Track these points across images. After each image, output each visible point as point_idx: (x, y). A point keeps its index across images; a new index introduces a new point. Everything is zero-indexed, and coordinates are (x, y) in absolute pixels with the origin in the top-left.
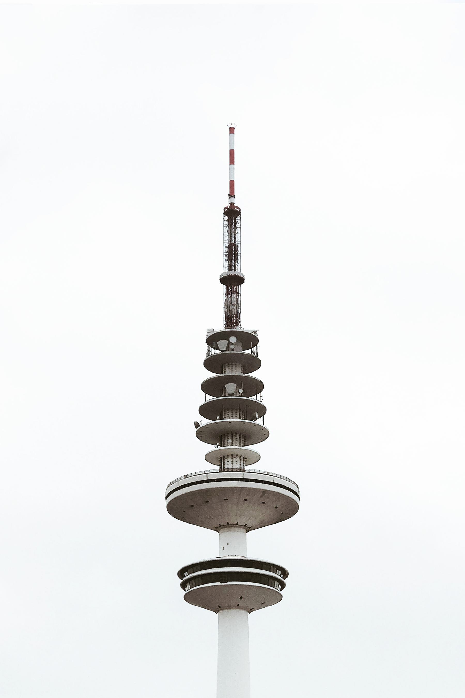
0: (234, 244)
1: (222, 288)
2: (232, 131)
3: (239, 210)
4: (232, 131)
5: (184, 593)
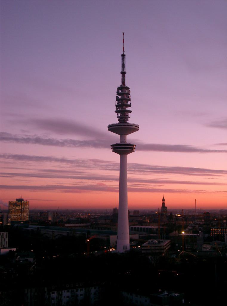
1: (121, 75)
2: (123, 34)
4: (123, 34)
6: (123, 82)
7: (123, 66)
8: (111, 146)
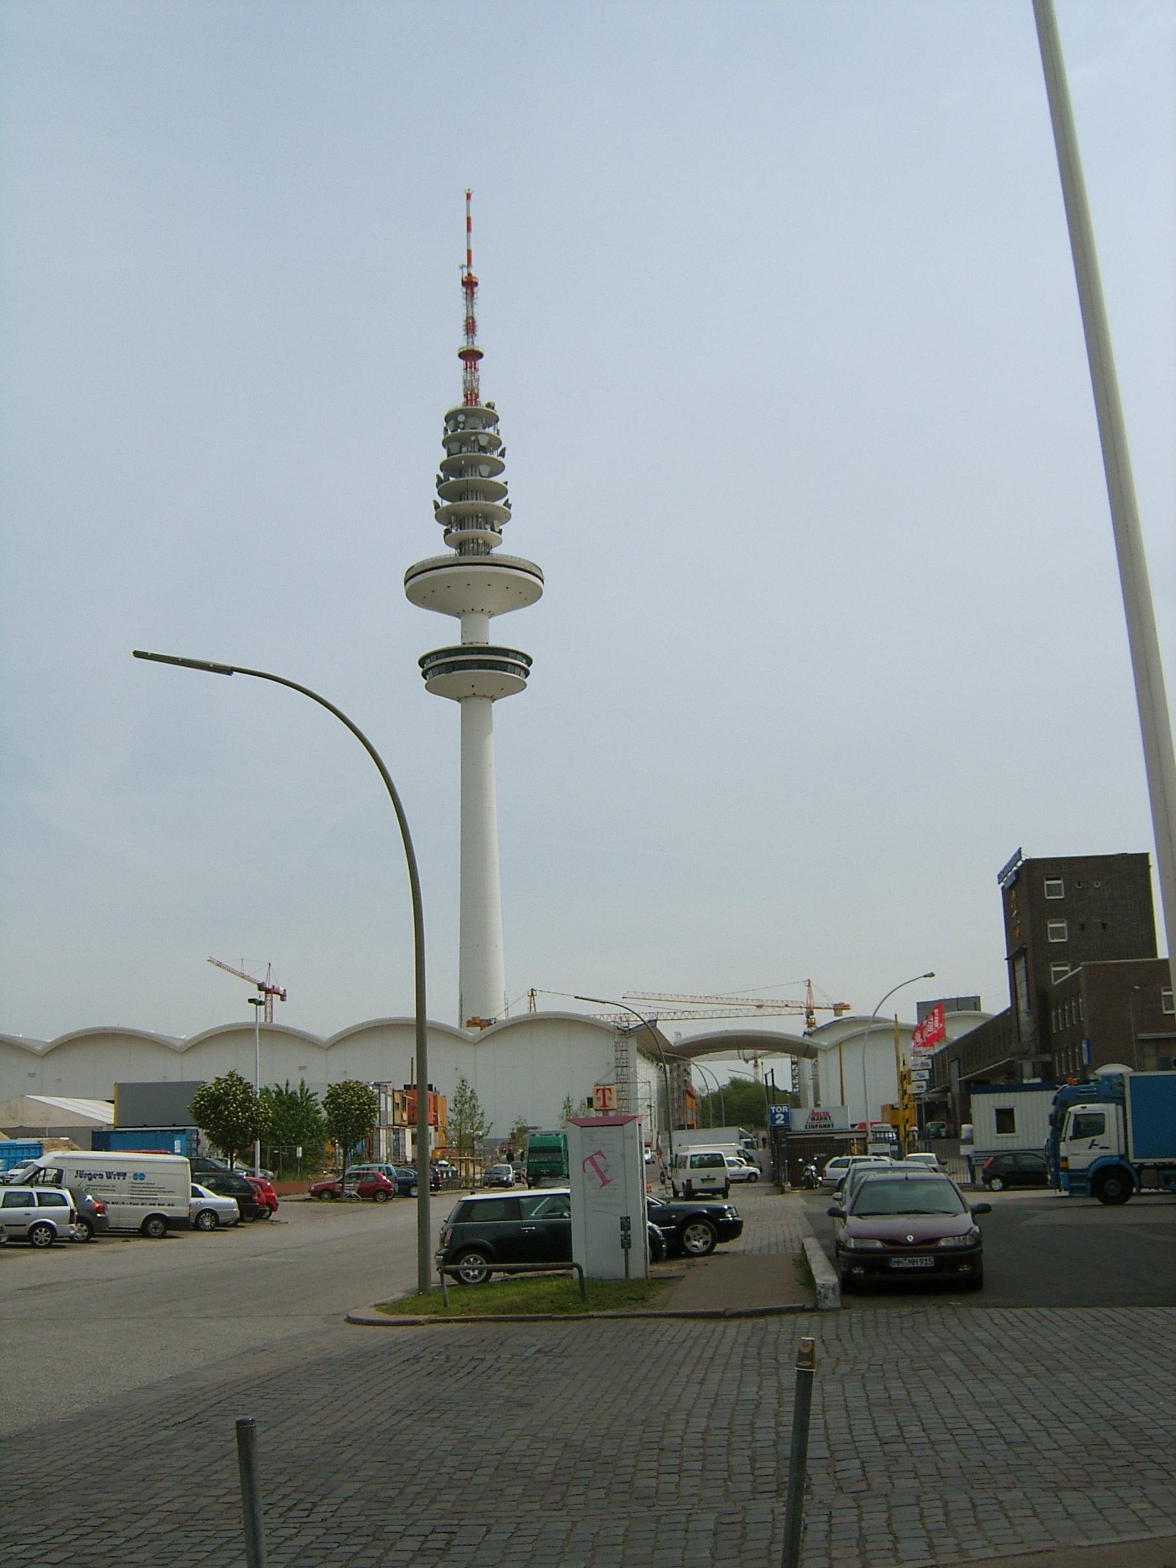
0: (473, 318)
1: (462, 363)
2: (469, 196)
3: (264, 1216)
4: (469, 196)
5: (426, 682)
6: (471, 395)
7: (470, 327)
8: (411, 575)
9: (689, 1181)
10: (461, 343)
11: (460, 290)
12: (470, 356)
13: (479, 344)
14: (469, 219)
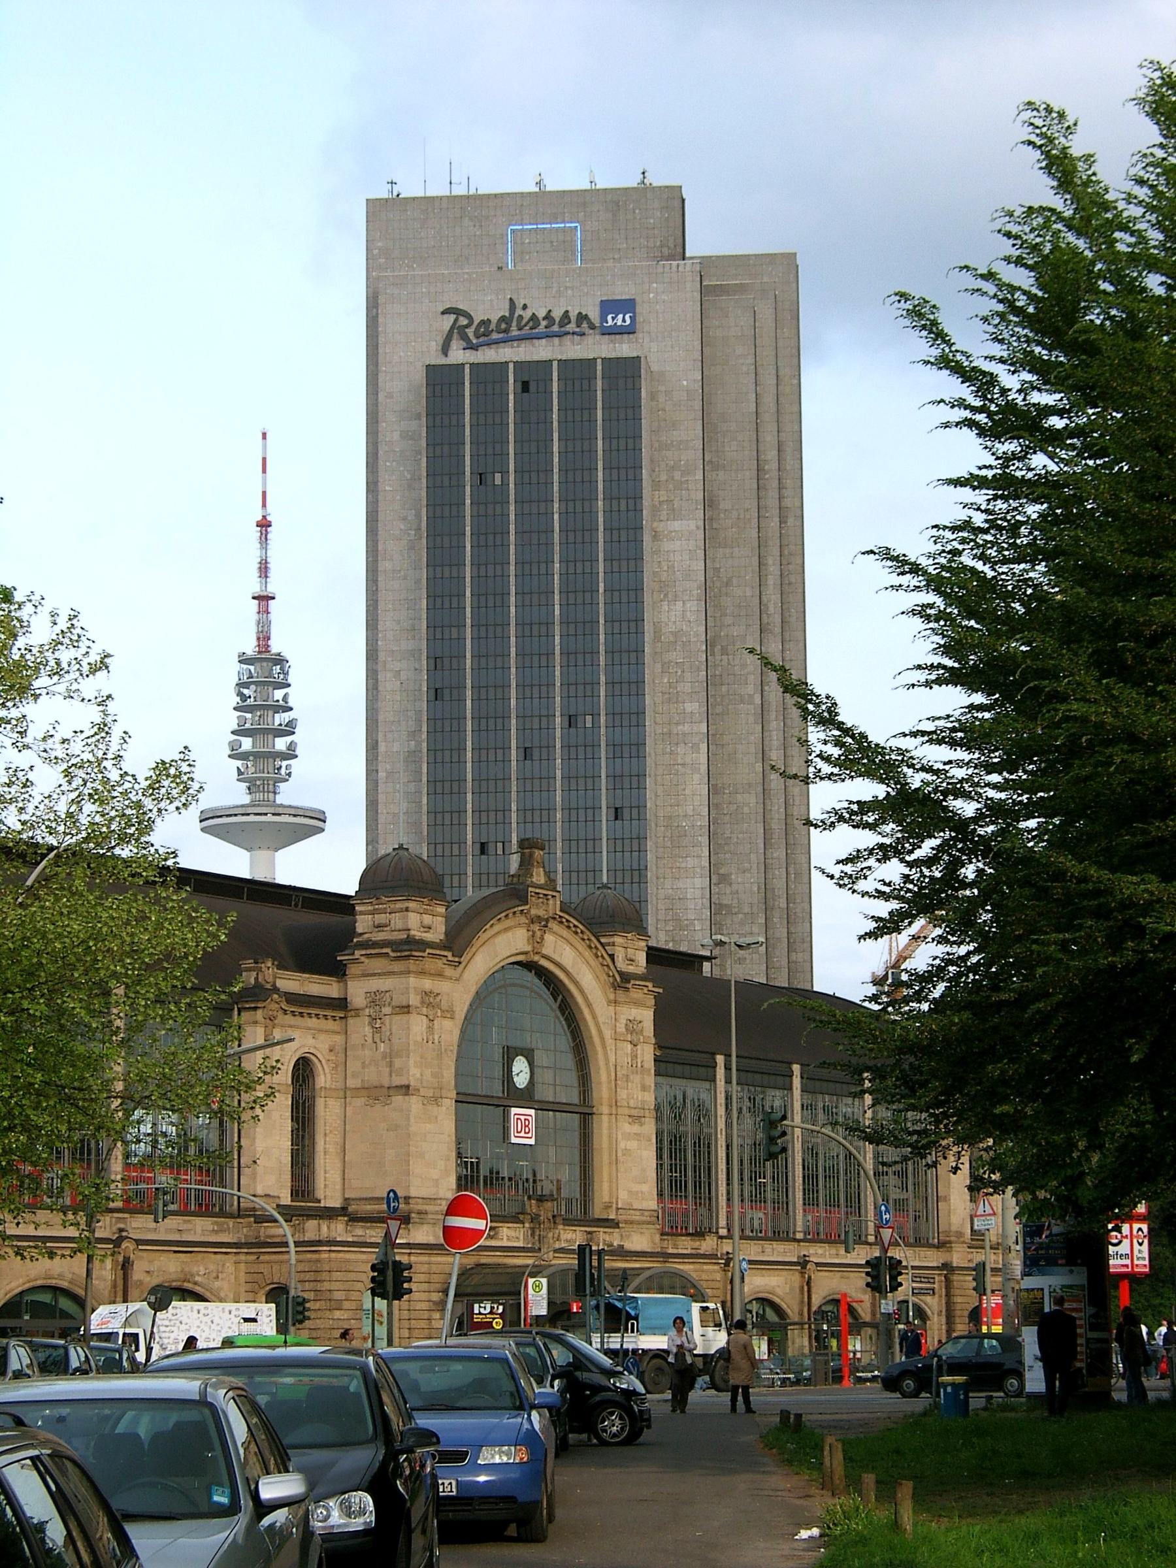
2: (264, 436)
4: (264, 436)
6: (264, 638)
7: (264, 569)
9: (847, 1251)
10: (256, 588)
11: (255, 532)
12: (264, 599)
13: (271, 589)
14: (264, 471)
